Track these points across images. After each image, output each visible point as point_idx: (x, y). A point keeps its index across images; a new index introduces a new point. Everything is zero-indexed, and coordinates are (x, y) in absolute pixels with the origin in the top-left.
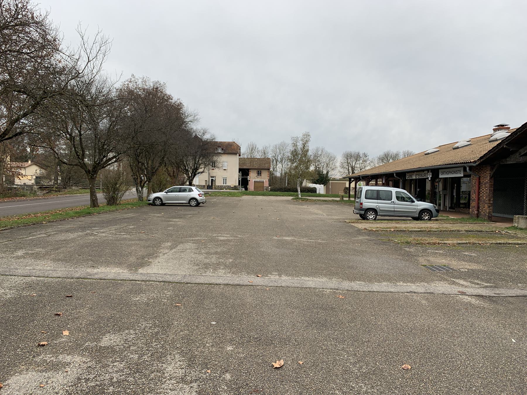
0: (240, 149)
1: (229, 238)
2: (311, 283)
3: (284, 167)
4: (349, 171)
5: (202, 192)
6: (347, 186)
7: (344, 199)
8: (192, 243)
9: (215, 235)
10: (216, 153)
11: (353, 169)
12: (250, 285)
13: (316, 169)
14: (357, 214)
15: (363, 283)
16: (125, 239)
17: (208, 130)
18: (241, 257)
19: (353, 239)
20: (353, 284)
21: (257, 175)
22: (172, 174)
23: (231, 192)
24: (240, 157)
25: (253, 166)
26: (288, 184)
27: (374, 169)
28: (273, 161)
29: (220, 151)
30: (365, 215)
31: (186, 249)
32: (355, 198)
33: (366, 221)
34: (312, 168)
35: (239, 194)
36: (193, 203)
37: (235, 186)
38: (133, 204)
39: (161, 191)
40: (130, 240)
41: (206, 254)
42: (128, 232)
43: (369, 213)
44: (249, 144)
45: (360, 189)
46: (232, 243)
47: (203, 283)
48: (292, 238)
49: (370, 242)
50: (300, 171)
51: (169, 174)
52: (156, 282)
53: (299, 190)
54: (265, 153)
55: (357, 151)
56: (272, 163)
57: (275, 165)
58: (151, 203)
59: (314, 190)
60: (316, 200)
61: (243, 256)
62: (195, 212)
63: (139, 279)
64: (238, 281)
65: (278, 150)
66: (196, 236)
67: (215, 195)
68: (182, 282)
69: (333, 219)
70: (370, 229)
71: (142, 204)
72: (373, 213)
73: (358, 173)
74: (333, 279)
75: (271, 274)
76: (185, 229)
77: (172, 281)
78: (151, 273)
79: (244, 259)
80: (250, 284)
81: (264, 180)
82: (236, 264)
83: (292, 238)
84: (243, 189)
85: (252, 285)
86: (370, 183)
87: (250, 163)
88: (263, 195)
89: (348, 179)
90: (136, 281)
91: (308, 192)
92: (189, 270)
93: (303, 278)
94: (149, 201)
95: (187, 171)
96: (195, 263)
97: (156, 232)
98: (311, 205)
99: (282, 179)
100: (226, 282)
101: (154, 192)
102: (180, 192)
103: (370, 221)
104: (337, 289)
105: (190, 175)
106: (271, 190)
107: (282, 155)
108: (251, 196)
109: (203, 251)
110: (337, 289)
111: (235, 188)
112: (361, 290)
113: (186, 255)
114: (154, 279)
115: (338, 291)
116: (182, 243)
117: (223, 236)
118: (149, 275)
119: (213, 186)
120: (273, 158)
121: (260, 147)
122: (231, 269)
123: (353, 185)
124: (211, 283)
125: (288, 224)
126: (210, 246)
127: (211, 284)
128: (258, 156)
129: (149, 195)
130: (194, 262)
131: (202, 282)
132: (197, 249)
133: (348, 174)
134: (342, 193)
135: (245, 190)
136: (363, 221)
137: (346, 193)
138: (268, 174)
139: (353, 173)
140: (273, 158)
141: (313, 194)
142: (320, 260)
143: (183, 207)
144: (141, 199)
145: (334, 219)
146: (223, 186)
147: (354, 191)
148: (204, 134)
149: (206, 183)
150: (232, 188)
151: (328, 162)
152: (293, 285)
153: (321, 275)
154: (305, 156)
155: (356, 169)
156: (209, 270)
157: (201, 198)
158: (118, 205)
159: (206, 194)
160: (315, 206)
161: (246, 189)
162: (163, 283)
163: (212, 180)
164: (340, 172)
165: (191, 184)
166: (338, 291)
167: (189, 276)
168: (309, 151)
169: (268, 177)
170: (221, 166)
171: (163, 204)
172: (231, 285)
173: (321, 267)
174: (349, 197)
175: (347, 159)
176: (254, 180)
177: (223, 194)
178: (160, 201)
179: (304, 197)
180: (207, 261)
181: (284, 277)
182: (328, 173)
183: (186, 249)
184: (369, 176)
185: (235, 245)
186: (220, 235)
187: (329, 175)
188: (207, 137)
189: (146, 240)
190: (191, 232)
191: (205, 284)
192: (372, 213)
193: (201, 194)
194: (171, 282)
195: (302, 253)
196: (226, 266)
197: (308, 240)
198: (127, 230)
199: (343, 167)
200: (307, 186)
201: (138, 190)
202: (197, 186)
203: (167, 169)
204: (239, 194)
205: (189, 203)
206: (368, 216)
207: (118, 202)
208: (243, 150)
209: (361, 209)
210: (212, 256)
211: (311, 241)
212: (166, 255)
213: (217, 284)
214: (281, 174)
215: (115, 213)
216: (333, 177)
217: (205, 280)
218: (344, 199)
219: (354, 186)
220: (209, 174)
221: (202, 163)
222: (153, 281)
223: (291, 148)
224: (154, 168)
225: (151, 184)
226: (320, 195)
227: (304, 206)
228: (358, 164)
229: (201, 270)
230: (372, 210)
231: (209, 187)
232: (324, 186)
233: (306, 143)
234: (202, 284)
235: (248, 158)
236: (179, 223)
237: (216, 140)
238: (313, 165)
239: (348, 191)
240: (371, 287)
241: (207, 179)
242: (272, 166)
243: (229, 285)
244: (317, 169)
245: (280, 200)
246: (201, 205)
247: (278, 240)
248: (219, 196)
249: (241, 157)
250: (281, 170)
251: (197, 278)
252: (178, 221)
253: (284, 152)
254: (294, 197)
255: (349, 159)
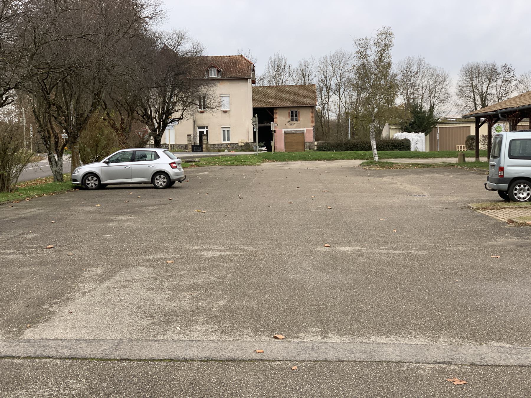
0: (253, 70)
1: (223, 253)
2: (391, 349)
3: (343, 101)
4: (475, 103)
5: (176, 157)
6: (473, 133)
7: (467, 159)
8: (147, 267)
9: (196, 248)
10: (206, 79)
11: (484, 98)
12: (256, 360)
13: (408, 101)
14: (493, 190)
15: (508, 345)
16: (12, 263)
17: (187, 34)
18: (244, 295)
19: (484, 244)
20: (484, 348)
21: (289, 119)
22: (118, 125)
23: (239, 156)
24: (254, 85)
25: (281, 102)
26: (353, 134)
27: (526, 96)
28: (321, 91)
29: (213, 74)
30: (510, 190)
31: (133, 281)
32: (489, 158)
33: (511, 204)
34: (399, 101)
35: (254, 159)
36: (161, 182)
37: (247, 144)
38: (42, 189)
39: (98, 160)
40: (22, 264)
41: (172, 289)
42: (21, 248)
43: (518, 188)
44: (271, 59)
45: (498, 139)
46: (229, 264)
47: (157, 358)
48: (357, 248)
49: (522, 248)
50: (374, 109)
51: (113, 126)
52: (57, 358)
53: (375, 147)
54: (303, 75)
55: (490, 61)
56: (318, 95)
57: (325, 99)
58: (78, 184)
59: (405, 145)
60: (409, 164)
61: (249, 291)
62: (161, 201)
63: (20, 355)
64: (232, 350)
65: (330, 68)
66: (157, 250)
67: (209, 163)
68: (112, 357)
69: (444, 203)
70: (521, 221)
71: (60, 188)
72: (527, 188)
73: (493, 106)
74: (440, 337)
75: (306, 332)
76: (137, 237)
77: (89, 357)
78: (49, 338)
79: (251, 298)
80: (258, 357)
81: (305, 129)
82: (232, 312)
83: (357, 248)
84: (264, 149)
85: (261, 360)
86: (519, 124)
87: (276, 95)
88: (304, 159)
89: (473, 118)
90: (13, 357)
91: (392, 149)
92: (130, 328)
93: (374, 338)
94: (75, 180)
95: (150, 117)
96: (145, 313)
97: (78, 245)
98: (399, 175)
99: (339, 125)
100: (205, 354)
101: (86, 162)
102: (133, 160)
103: (520, 203)
104: (450, 363)
105: (156, 125)
106: (319, 149)
107: (338, 77)
108: (279, 163)
109: (167, 284)
110: (450, 363)
111: (247, 147)
112: (503, 363)
113: (129, 294)
114: (53, 353)
115: (452, 368)
116: (127, 267)
117: (213, 250)
118: (42, 344)
119: (204, 146)
120: (322, 85)
121: (294, 64)
122: (220, 322)
123: (484, 130)
124: (172, 357)
125: (349, 217)
126: (182, 273)
127: (172, 360)
128: (290, 81)
129: (74, 170)
130: (143, 309)
131: (155, 356)
132: (156, 279)
133: (473, 108)
134: (463, 149)
135: (268, 151)
136: (507, 205)
137: (470, 147)
138: (312, 117)
139: (484, 105)
140: (322, 85)
141: (403, 152)
142: (414, 296)
143: (141, 190)
144: (59, 178)
145: (446, 203)
146: (222, 144)
147: (487, 142)
148: (179, 42)
149: (190, 141)
150: (240, 148)
151: (432, 87)
152: (352, 357)
153: (415, 330)
154: (385, 75)
155: (489, 97)
156: (174, 327)
157: (176, 170)
158: (11, 191)
159: (187, 162)
160: (407, 176)
161: (269, 149)
162: (69, 362)
163: (201, 133)
164: (457, 105)
165: (158, 145)
166: (452, 368)
167: (129, 342)
168: (392, 66)
169: (312, 122)
170: (215, 104)
171: (102, 187)
172: (217, 361)
173: (414, 310)
174: (477, 156)
175: (471, 79)
176: (283, 130)
177: (223, 161)
178: (96, 180)
179: (385, 160)
180: (173, 305)
181: (333, 339)
182: (432, 108)
183: (133, 281)
184: (514, 111)
185: (234, 268)
186: (206, 247)
187: (435, 112)
188: (185, 48)
189: (54, 263)
190: (147, 243)
191: (161, 360)
192: (525, 186)
193: (174, 163)
194: (86, 359)
195: (374, 280)
196: (210, 316)
197: (390, 251)
198: (20, 243)
199: (462, 95)
200: (391, 137)
201: (52, 159)
202: (173, 146)
203: (108, 115)
204: (254, 159)
205: (152, 181)
206: (516, 194)
207: (12, 186)
208: (260, 72)
209: (501, 180)
210: (184, 293)
211: (395, 252)
212: (87, 297)
213: (185, 360)
214: (339, 115)
215: (5, 209)
216: (443, 116)
217: (162, 352)
218: (467, 159)
219: (486, 133)
220: (195, 122)
221: (177, 102)
222: (49, 357)
223: (354, 62)
224: (82, 115)
225: (77, 147)
226: (418, 155)
227: (385, 179)
228: (493, 87)
229: (154, 327)
230: (524, 181)
231: (197, 148)
232: (426, 135)
233: (384, 50)
234: (154, 360)
235: (270, 86)
236: (126, 224)
237: (205, 54)
238: (402, 93)
239: (474, 144)
240: (525, 355)
241: (191, 132)
242: (320, 101)
243: (212, 360)
244: (411, 101)
245: (338, 168)
246: (177, 184)
247: (326, 254)
248: (215, 165)
249: (257, 84)
250: (336, 107)
251: (144, 347)
252: (127, 220)
253: (343, 71)
254: (365, 161)
255: (475, 79)
